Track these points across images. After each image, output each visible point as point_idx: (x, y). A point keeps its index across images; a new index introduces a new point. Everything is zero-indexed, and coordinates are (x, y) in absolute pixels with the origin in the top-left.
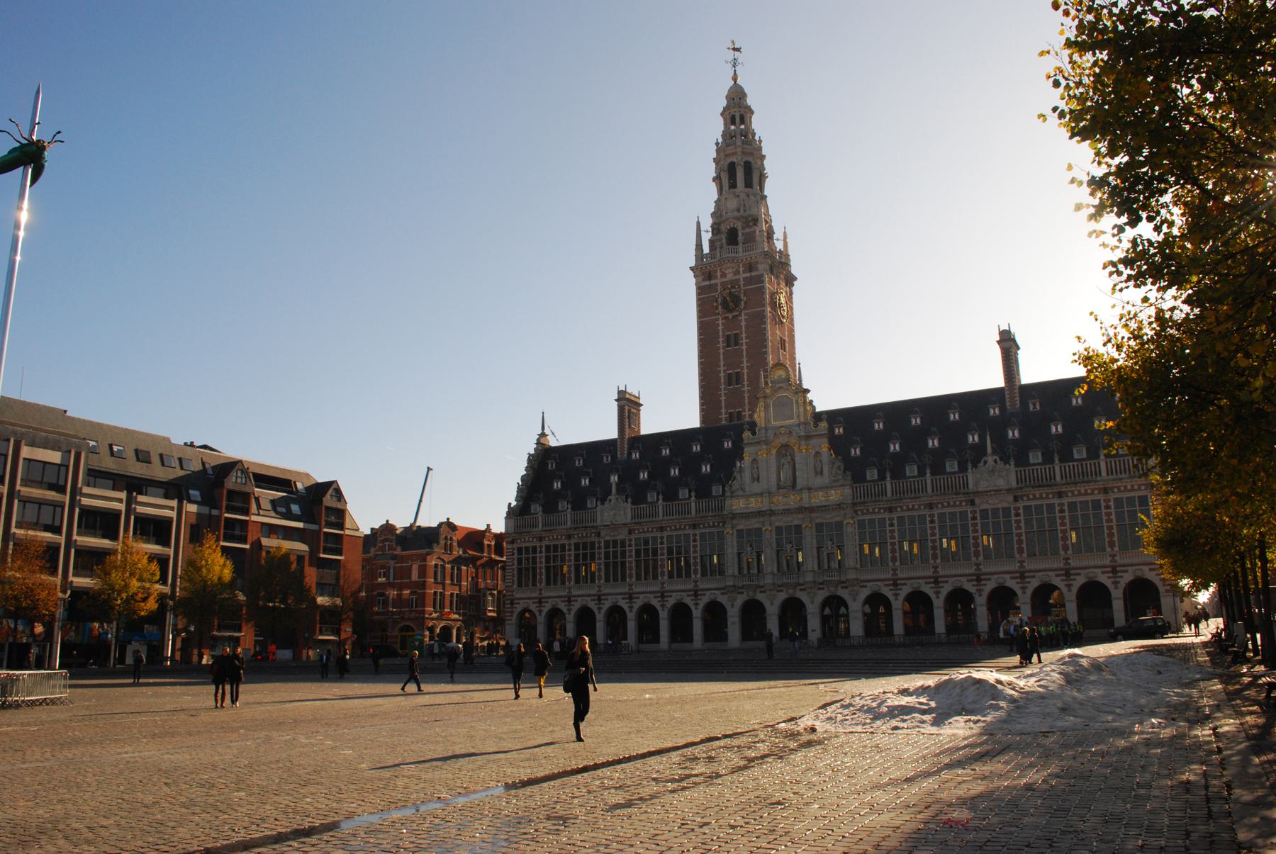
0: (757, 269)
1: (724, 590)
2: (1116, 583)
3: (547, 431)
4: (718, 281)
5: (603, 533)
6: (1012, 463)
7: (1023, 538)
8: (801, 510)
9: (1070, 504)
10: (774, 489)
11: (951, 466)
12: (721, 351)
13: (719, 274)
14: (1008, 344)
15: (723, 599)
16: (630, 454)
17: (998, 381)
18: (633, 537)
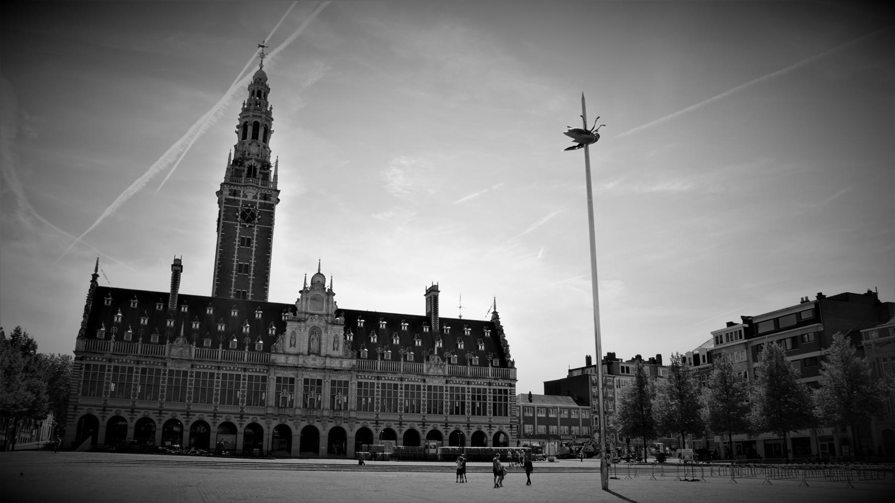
0: (270, 200)
1: (264, 416)
2: (401, 430)
4: (241, 199)
5: (168, 364)
6: (195, 343)
8: (324, 369)
9: (473, 389)
10: (306, 353)
11: (155, 338)
12: (237, 247)
13: (242, 194)
14: (432, 295)
15: (261, 422)
16: (179, 308)
17: (167, 289)
18: (195, 370)
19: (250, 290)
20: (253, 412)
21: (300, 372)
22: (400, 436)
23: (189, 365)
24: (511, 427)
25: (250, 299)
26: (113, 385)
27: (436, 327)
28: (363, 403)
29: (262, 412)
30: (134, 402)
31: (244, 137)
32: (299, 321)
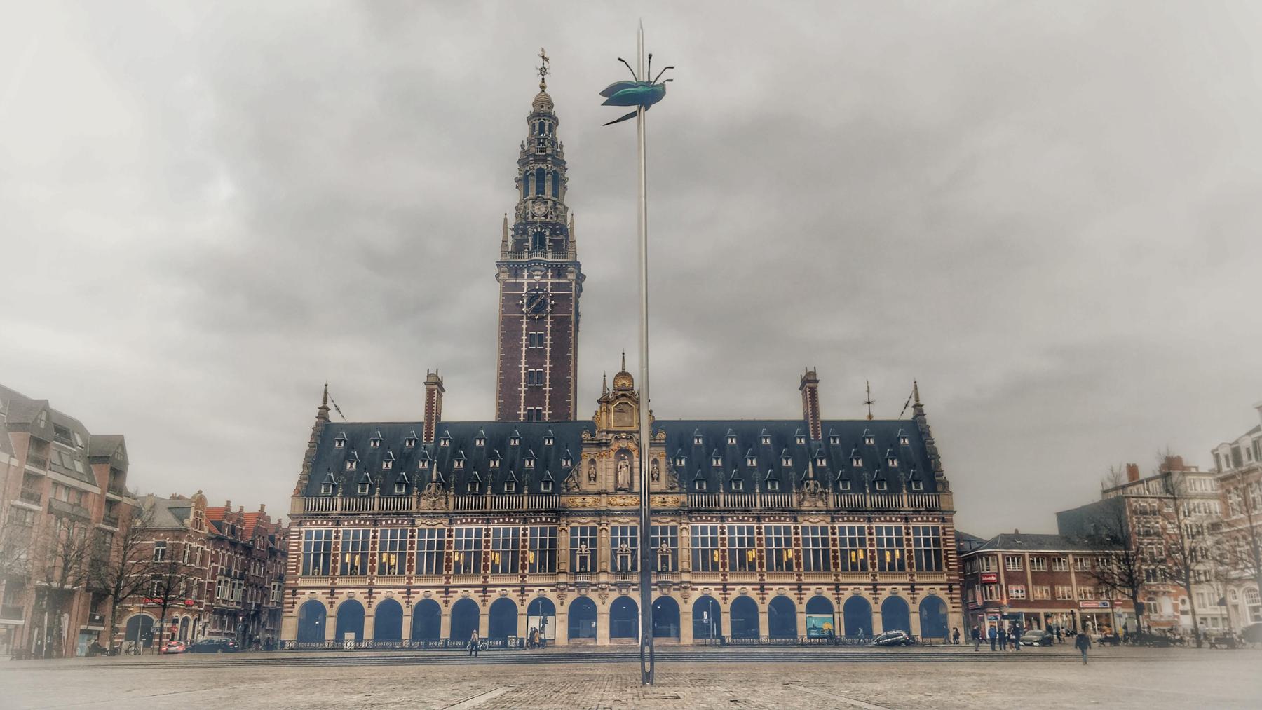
0: (566, 277)
3: (329, 405)
7: (415, 557)
10: (611, 489)
12: (524, 349)
13: (526, 274)
14: (810, 385)
19: (547, 407)
20: (540, 582)
21: (604, 520)
22: (839, 607)
23: (446, 522)
24: (950, 589)
25: (547, 418)
26: (532, 555)
27: (816, 437)
28: (888, 559)
29: (552, 581)
30: (874, 576)
31: (526, 193)
32: (599, 445)
